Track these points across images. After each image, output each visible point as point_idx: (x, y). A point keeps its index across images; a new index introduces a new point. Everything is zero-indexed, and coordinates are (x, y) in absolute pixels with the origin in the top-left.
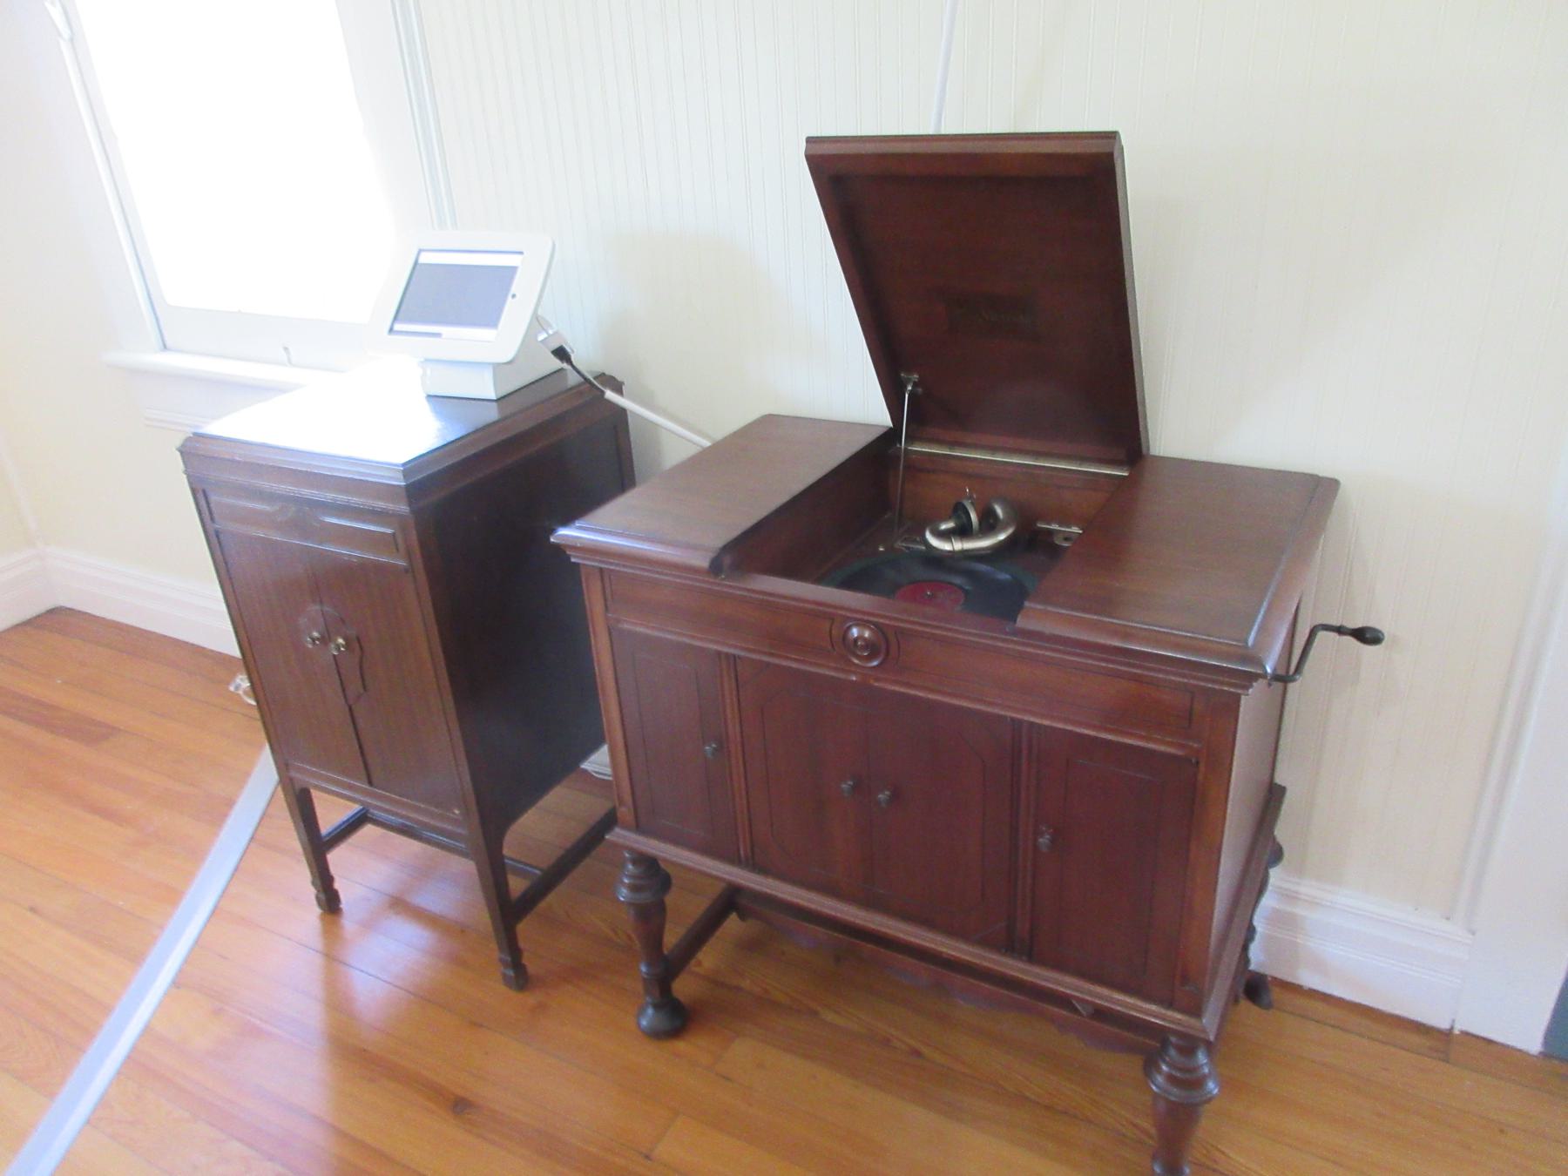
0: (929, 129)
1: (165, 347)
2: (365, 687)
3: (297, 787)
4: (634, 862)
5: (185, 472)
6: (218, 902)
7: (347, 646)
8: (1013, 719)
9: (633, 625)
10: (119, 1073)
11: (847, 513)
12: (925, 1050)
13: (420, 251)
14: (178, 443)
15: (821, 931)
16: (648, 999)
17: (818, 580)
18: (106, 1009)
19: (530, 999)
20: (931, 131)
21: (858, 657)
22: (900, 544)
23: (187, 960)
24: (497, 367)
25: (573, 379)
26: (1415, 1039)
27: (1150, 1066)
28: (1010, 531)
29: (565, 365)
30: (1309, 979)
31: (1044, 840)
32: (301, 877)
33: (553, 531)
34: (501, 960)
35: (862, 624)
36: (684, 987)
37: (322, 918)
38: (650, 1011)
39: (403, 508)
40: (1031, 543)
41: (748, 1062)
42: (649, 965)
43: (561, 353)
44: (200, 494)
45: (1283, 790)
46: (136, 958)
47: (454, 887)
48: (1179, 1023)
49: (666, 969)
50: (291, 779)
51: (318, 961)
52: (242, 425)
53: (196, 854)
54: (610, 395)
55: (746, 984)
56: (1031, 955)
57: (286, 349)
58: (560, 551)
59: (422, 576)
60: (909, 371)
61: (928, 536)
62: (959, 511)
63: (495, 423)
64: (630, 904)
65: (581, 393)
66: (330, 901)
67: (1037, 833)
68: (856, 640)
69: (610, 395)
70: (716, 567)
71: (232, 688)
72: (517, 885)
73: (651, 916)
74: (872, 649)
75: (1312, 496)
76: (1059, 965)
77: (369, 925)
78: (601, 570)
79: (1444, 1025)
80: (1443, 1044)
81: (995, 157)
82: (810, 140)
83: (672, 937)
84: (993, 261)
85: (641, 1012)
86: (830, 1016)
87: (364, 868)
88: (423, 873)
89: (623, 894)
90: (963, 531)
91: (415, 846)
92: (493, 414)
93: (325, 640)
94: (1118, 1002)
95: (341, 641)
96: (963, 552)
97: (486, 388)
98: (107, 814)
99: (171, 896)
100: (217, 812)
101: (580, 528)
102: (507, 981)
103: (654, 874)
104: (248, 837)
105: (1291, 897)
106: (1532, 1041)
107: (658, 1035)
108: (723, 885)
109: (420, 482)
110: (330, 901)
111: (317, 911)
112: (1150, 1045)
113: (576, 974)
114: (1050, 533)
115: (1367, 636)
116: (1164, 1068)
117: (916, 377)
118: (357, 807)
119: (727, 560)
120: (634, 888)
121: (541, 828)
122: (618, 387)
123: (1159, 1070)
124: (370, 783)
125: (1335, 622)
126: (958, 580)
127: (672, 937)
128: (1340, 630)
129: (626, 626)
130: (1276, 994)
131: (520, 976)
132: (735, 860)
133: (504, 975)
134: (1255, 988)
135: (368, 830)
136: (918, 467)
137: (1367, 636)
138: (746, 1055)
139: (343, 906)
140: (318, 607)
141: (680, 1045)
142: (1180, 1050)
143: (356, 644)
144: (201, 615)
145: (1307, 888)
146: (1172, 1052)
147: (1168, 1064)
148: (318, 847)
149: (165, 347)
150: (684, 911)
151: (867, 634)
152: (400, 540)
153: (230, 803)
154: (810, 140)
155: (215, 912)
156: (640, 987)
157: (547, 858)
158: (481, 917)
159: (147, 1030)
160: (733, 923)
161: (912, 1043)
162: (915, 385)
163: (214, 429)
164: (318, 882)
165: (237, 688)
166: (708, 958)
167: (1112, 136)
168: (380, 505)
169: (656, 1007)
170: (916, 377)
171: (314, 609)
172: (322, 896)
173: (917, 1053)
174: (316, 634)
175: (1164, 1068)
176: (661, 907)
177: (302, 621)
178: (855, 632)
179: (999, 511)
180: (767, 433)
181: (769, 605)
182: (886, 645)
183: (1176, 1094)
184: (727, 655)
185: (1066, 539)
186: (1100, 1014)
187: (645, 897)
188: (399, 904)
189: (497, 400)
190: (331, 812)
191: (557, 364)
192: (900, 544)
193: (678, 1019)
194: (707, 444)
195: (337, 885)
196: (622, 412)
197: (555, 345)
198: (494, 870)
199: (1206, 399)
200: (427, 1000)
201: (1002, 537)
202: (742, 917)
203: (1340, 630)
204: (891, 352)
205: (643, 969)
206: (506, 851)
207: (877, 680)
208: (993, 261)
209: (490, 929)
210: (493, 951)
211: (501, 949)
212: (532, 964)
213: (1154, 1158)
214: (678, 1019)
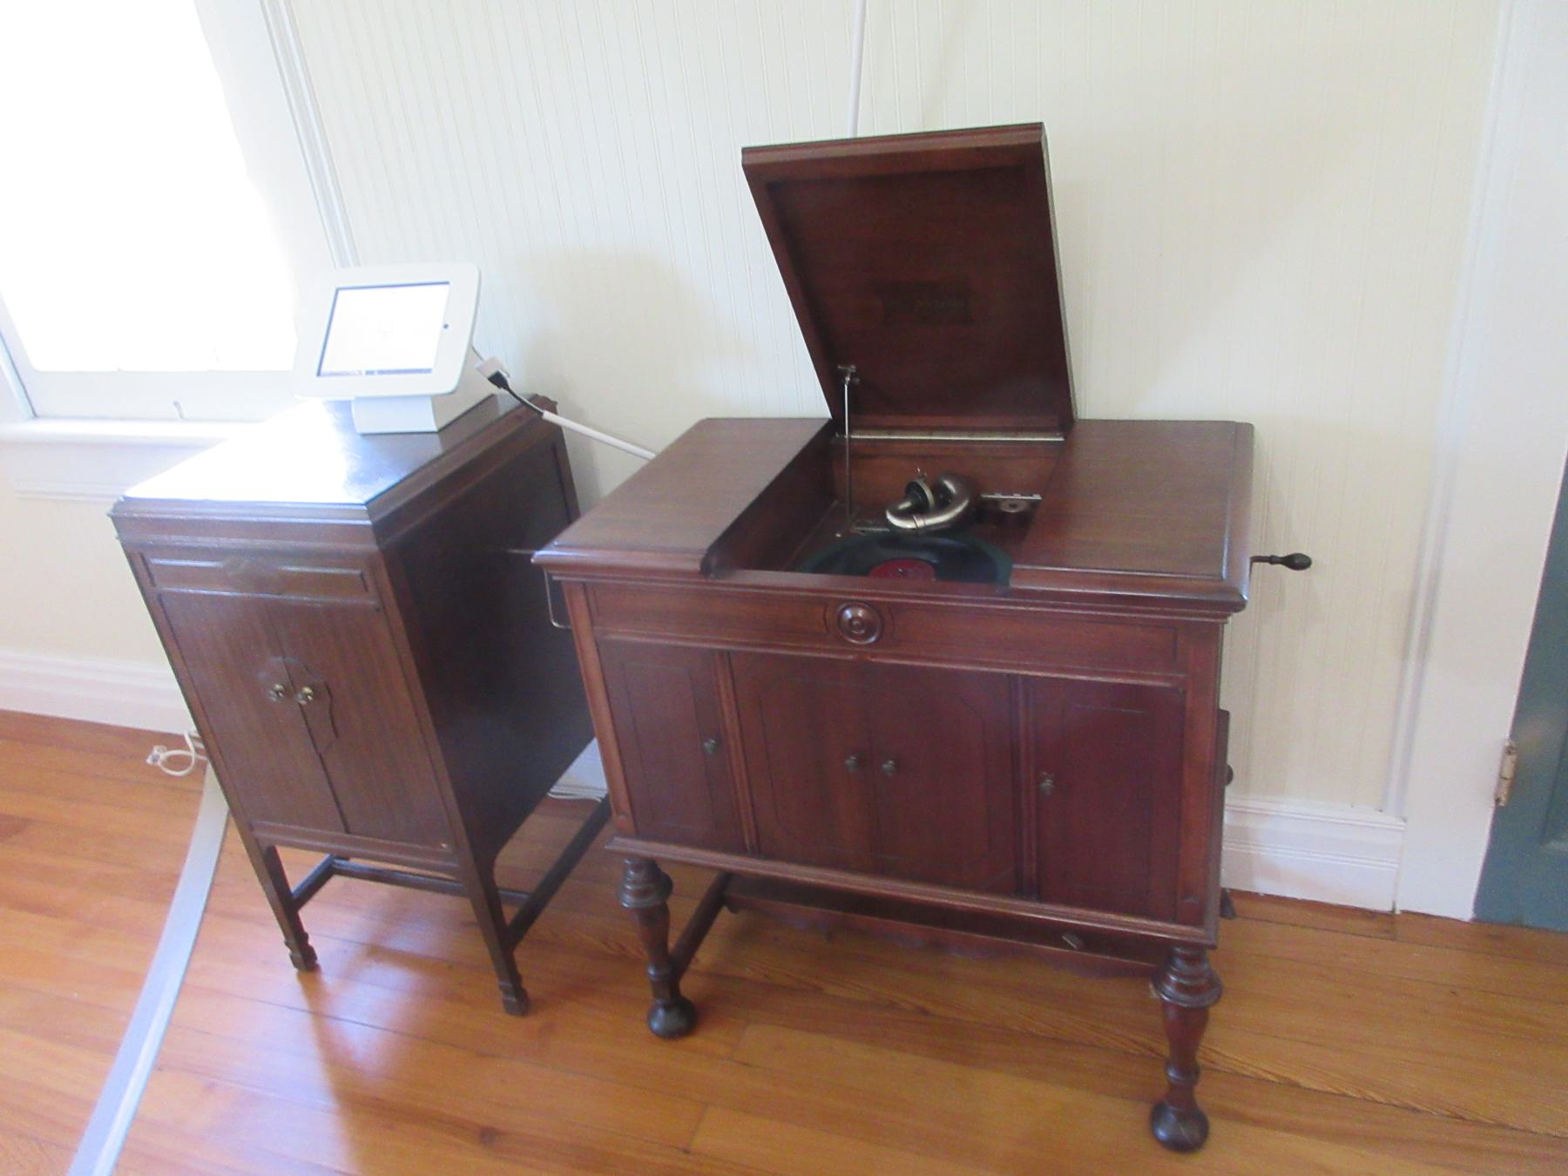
0: (847, 135)
1: (35, 416)
2: (336, 733)
3: (265, 845)
4: (637, 868)
5: (120, 537)
6: (184, 977)
7: (316, 694)
8: (1009, 675)
9: (623, 635)
10: (117, 1166)
11: (804, 505)
12: (930, 1007)
13: (337, 291)
14: (109, 508)
15: (814, 911)
16: (659, 1001)
17: (792, 568)
18: (89, 1106)
19: (535, 1022)
20: (848, 135)
21: (855, 637)
22: (857, 529)
23: (165, 1041)
24: (438, 401)
25: (506, 403)
26: (1364, 924)
27: (1158, 978)
28: (965, 504)
29: (502, 391)
30: (1264, 886)
31: (1047, 784)
32: (275, 936)
33: (530, 556)
34: (501, 988)
35: (852, 604)
36: (690, 986)
37: (300, 977)
38: (661, 1013)
39: (372, 547)
40: (982, 514)
41: (752, 1050)
42: (657, 968)
43: (498, 380)
44: (138, 559)
45: (1226, 714)
46: (109, 1048)
47: (435, 923)
48: (1182, 934)
49: (673, 967)
50: (257, 840)
51: (306, 1020)
52: (163, 486)
53: (149, 936)
54: (547, 415)
55: (748, 972)
56: (1038, 892)
57: (176, 404)
58: (539, 568)
59: (395, 614)
60: (847, 362)
61: (889, 517)
62: (912, 490)
63: (438, 459)
64: (636, 910)
65: (519, 418)
66: (306, 960)
67: (1040, 780)
68: (851, 620)
69: (547, 415)
70: (706, 569)
71: (149, 761)
72: (510, 913)
73: (654, 919)
74: (867, 627)
75: (1232, 441)
76: (1069, 901)
77: (349, 976)
78: (584, 584)
79: (1387, 908)
80: (1387, 923)
81: (929, 154)
82: (746, 151)
83: (674, 939)
84: (923, 255)
85: (651, 1015)
86: (831, 990)
87: (333, 923)
88: (395, 917)
89: (628, 901)
90: (920, 509)
91: (383, 890)
92: (435, 448)
93: (289, 692)
94: (1127, 925)
95: (307, 690)
96: (926, 528)
97: (428, 422)
98: (38, 908)
99: (133, 981)
100: (162, 889)
101: (559, 547)
102: (510, 1009)
103: (657, 879)
104: (202, 908)
105: (1242, 813)
106: (1463, 909)
107: (671, 1035)
108: (714, 875)
109: (380, 521)
110: (306, 960)
111: (294, 971)
112: (1150, 958)
113: (579, 989)
114: (996, 502)
115: (1297, 562)
116: (1173, 978)
117: (852, 369)
118: (325, 857)
119: (714, 561)
120: (641, 894)
121: (524, 855)
122: (552, 408)
123: (1168, 981)
124: (347, 831)
125: (1282, 553)
126: (925, 556)
127: (674, 939)
128: (1272, 560)
129: (614, 637)
130: (1236, 903)
131: (520, 1001)
132: (741, 850)
133: (506, 1003)
134: (1229, 902)
135: (336, 882)
136: (864, 454)
137: (1297, 562)
138: (761, 1040)
139: (320, 961)
140: (280, 659)
141: (696, 1041)
142: (1187, 959)
143: (324, 692)
144: (139, 687)
145: (1253, 803)
146: (1179, 962)
147: (1175, 974)
148: (288, 906)
149: (35, 416)
150: (683, 910)
151: (860, 613)
152: (369, 582)
153: (175, 878)
154: (746, 151)
155: (184, 988)
156: (648, 992)
157: (531, 885)
158: (478, 949)
159: (137, 1119)
160: (725, 917)
161: (921, 1003)
162: (853, 376)
163: (134, 492)
164: (293, 941)
165: (155, 760)
166: (705, 956)
167: (1037, 127)
168: (346, 546)
169: (667, 1008)
170: (852, 369)
171: (276, 661)
172: (299, 955)
173: (925, 1012)
174: (278, 687)
175: (1173, 978)
176: (664, 911)
177: (262, 675)
178: (848, 614)
179: (950, 486)
180: (708, 440)
181: (762, 597)
182: (883, 620)
183: (1185, 1000)
184: (721, 652)
185: (1013, 506)
186: (1092, 940)
187: (650, 901)
188: (376, 951)
189: (441, 431)
190: (298, 866)
191: (493, 389)
192: (857, 529)
193: (688, 1017)
194: (652, 456)
195: (311, 942)
196: (557, 429)
197: (491, 372)
198: (489, 900)
199: (1133, 358)
200: (422, 1039)
201: (959, 510)
202: (733, 909)
203: (1272, 560)
204: (828, 346)
205: (652, 972)
206: (497, 879)
207: (874, 656)
208: (923, 255)
209: (522, 943)
210: (493, 983)
211: (501, 977)
212: (532, 988)
213: (1168, 1064)
214: (688, 1017)
